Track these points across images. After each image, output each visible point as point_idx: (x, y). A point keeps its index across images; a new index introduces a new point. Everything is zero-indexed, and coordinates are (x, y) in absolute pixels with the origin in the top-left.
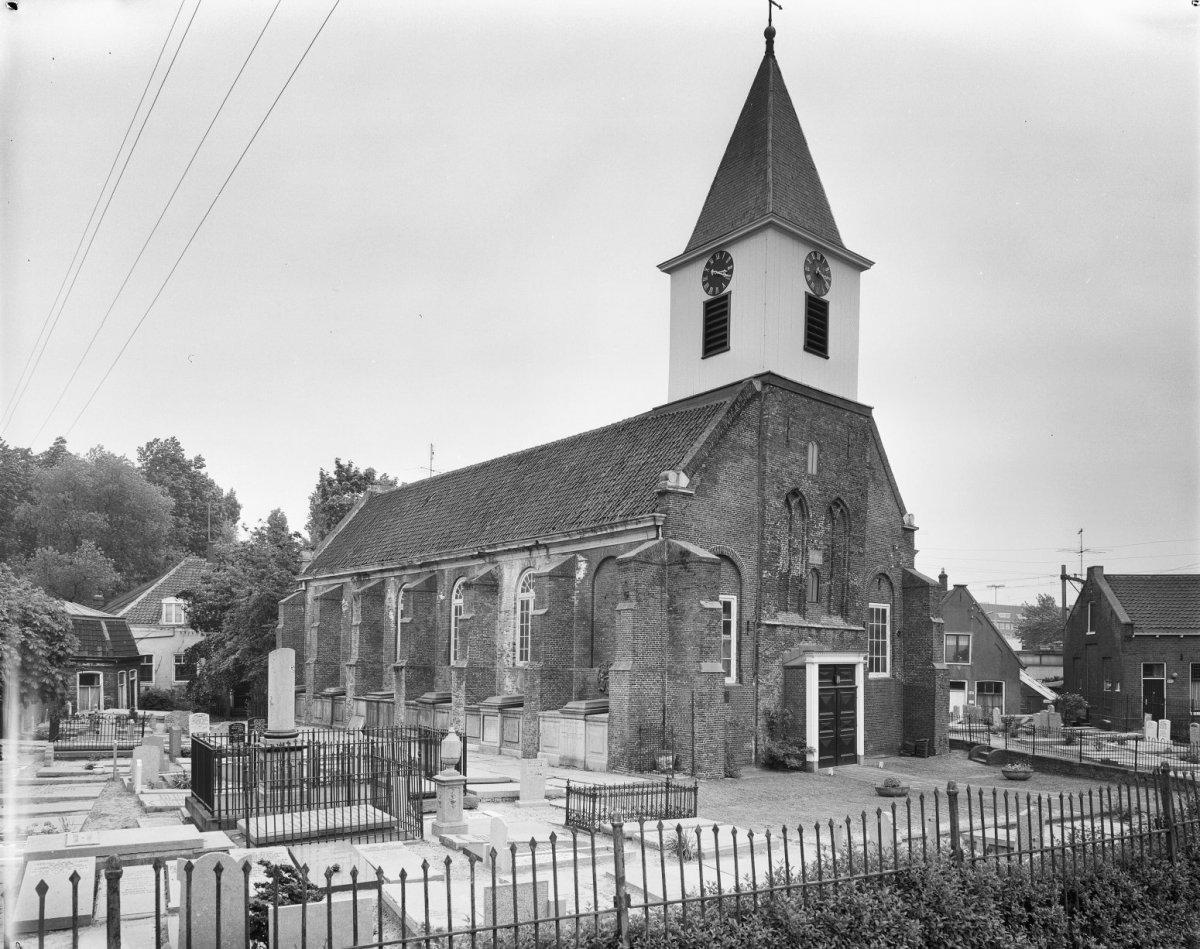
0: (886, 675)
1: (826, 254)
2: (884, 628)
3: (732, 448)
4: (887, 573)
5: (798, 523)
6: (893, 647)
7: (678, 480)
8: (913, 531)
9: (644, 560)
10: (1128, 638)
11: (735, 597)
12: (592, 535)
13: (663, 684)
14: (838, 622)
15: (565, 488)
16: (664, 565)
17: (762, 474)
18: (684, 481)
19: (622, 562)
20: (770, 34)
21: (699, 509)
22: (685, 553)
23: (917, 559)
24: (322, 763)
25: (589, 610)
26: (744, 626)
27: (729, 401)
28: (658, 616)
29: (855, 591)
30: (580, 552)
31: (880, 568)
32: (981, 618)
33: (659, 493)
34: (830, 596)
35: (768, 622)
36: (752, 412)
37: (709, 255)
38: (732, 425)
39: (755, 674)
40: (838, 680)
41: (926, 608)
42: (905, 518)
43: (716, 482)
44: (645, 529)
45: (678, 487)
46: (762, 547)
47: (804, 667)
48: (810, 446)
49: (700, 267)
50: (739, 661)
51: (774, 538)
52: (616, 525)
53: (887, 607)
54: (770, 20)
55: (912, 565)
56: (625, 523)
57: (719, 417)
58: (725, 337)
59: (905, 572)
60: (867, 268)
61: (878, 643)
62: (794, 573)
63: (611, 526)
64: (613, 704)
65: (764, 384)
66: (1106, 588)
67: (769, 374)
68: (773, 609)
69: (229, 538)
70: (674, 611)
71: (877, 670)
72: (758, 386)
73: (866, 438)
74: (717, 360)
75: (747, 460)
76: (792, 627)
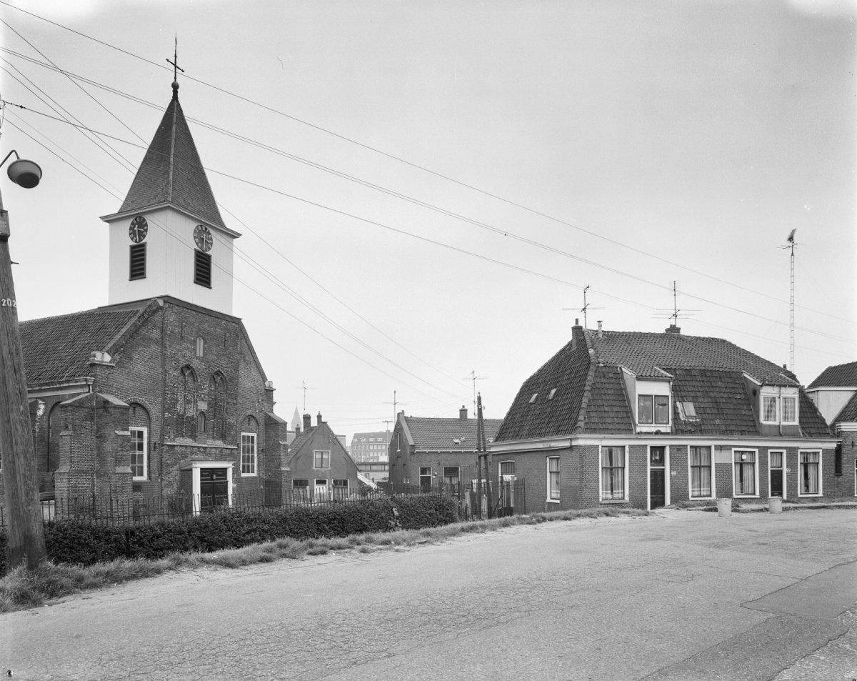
0: (255, 475)
3: (143, 339)
4: (254, 415)
5: (191, 385)
6: (259, 458)
7: (103, 357)
8: (272, 391)
9: (79, 405)
10: (412, 453)
12: (47, 387)
13: (93, 481)
14: (219, 443)
15: (34, 354)
16: (93, 409)
17: (164, 355)
18: (107, 358)
19: (63, 406)
21: (119, 377)
22: (106, 402)
23: (275, 408)
25: (46, 435)
27: (141, 310)
28: (90, 440)
29: (231, 426)
30: (41, 398)
31: (249, 412)
32: (335, 441)
33: (90, 364)
35: (168, 443)
36: (157, 318)
37: (134, 218)
38: (143, 324)
39: (160, 474)
40: (214, 477)
41: (277, 435)
42: (267, 383)
43: (131, 359)
44: (82, 386)
45: (102, 362)
46: (165, 399)
47: (191, 470)
48: (198, 341)
49: (128, 224)
50: (149, 466)
51: (173, 394)
52: (62, 382)
53: (255, 435)
54: (175, 78)
55: (272, 411)
56: (68, 381)
57: (134, 320)
58: (143, 269)
59: (266, 415)
61: (248, 456)
62: (188, 414)
63: (59, 383)
64: (57, 493)
65: (165, 302)
66: (404, 425)
67: (167, 296)
68: (172, 436)
70: (100, 437)
71: (248, 472)
72: (161, 303)
73: (237, 336)
74: (138, 283)
75: (153, 347)
76: (186, 447)
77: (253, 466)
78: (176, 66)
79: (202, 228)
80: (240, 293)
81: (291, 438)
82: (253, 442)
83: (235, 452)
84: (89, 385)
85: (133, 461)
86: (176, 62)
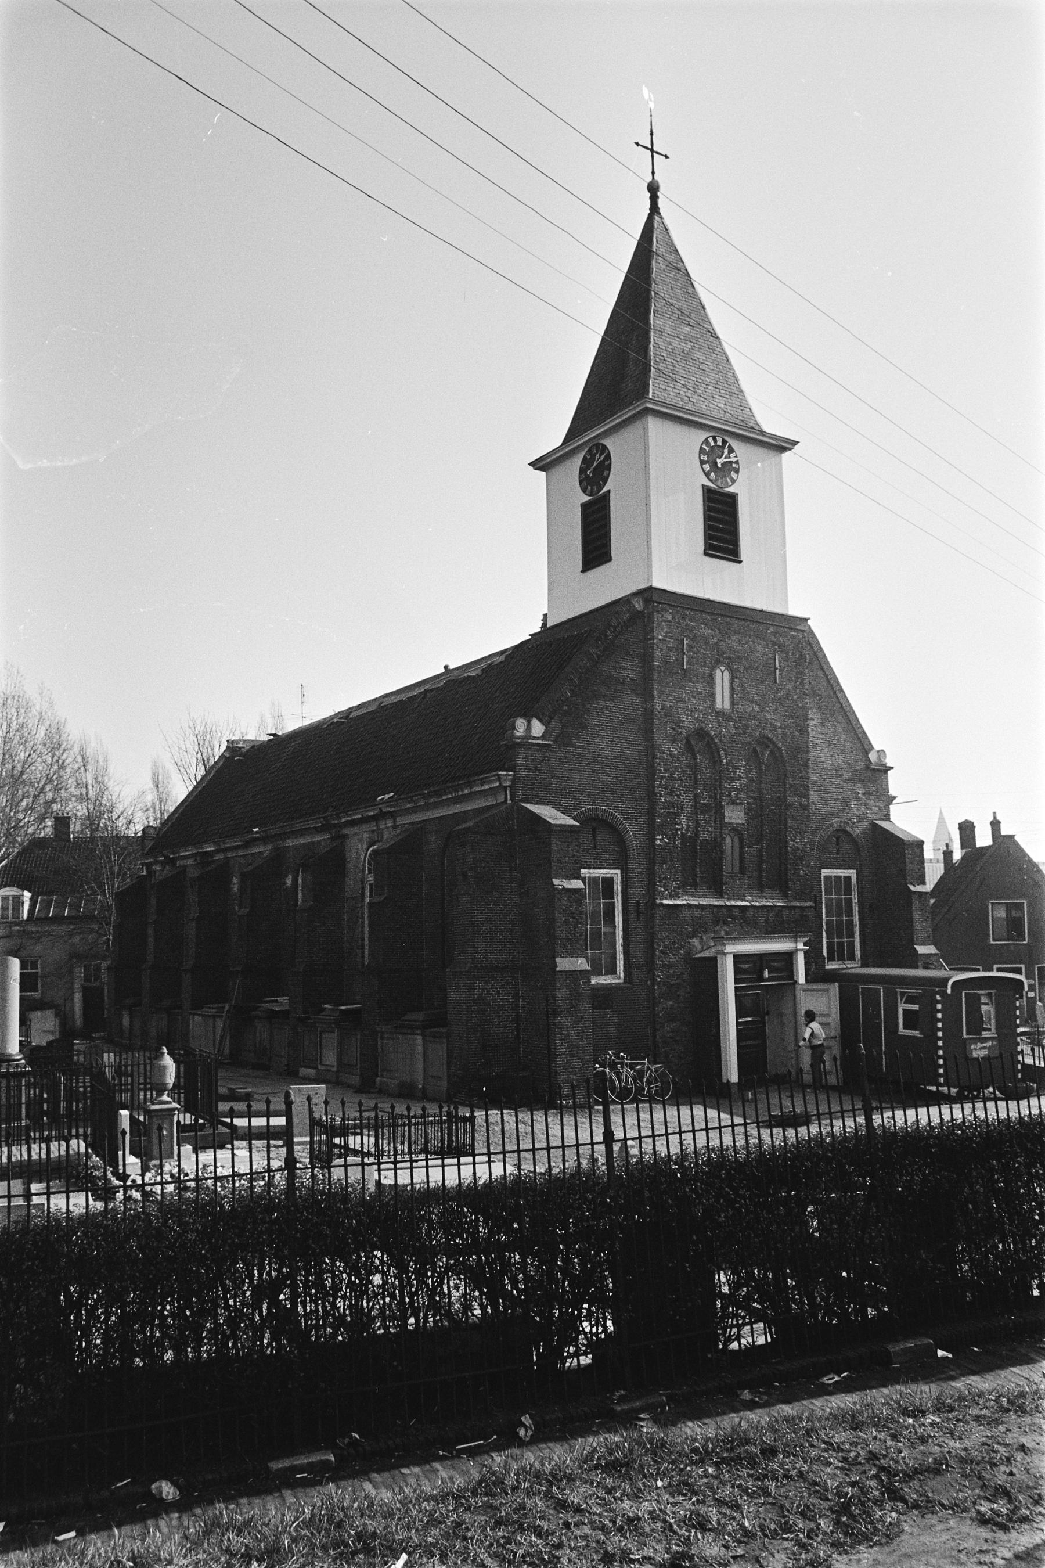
0: (732, 948)
1: (731, 438)
2: (849, 902)
7: (529, 727)
11: (618, 871)
12: (436, 800)
20: (653, 189)
24: (259, 1122)
26: (632, 908)
34: (760, 864)
37: (587, 458)
40: (766, 974)
42: (873, 756)
43: (584, 727)
48: (718, 672)
49: (576, 463)
51: (671, 793)
54: (653, 173)
55: (887, 817)
60: (790, 449)
62: (704, 836)
69: (513, 736)
72: (639, 605)
73: (802, 657)
77: (851, 945)
78: (652, 150)
79: (715, 441)
80: (805, 569)
81: (934, 872)
82: (848, 892)
83: (811, 914)
84: (506, 787)
85: (597, 944)
86: (652, 156)
